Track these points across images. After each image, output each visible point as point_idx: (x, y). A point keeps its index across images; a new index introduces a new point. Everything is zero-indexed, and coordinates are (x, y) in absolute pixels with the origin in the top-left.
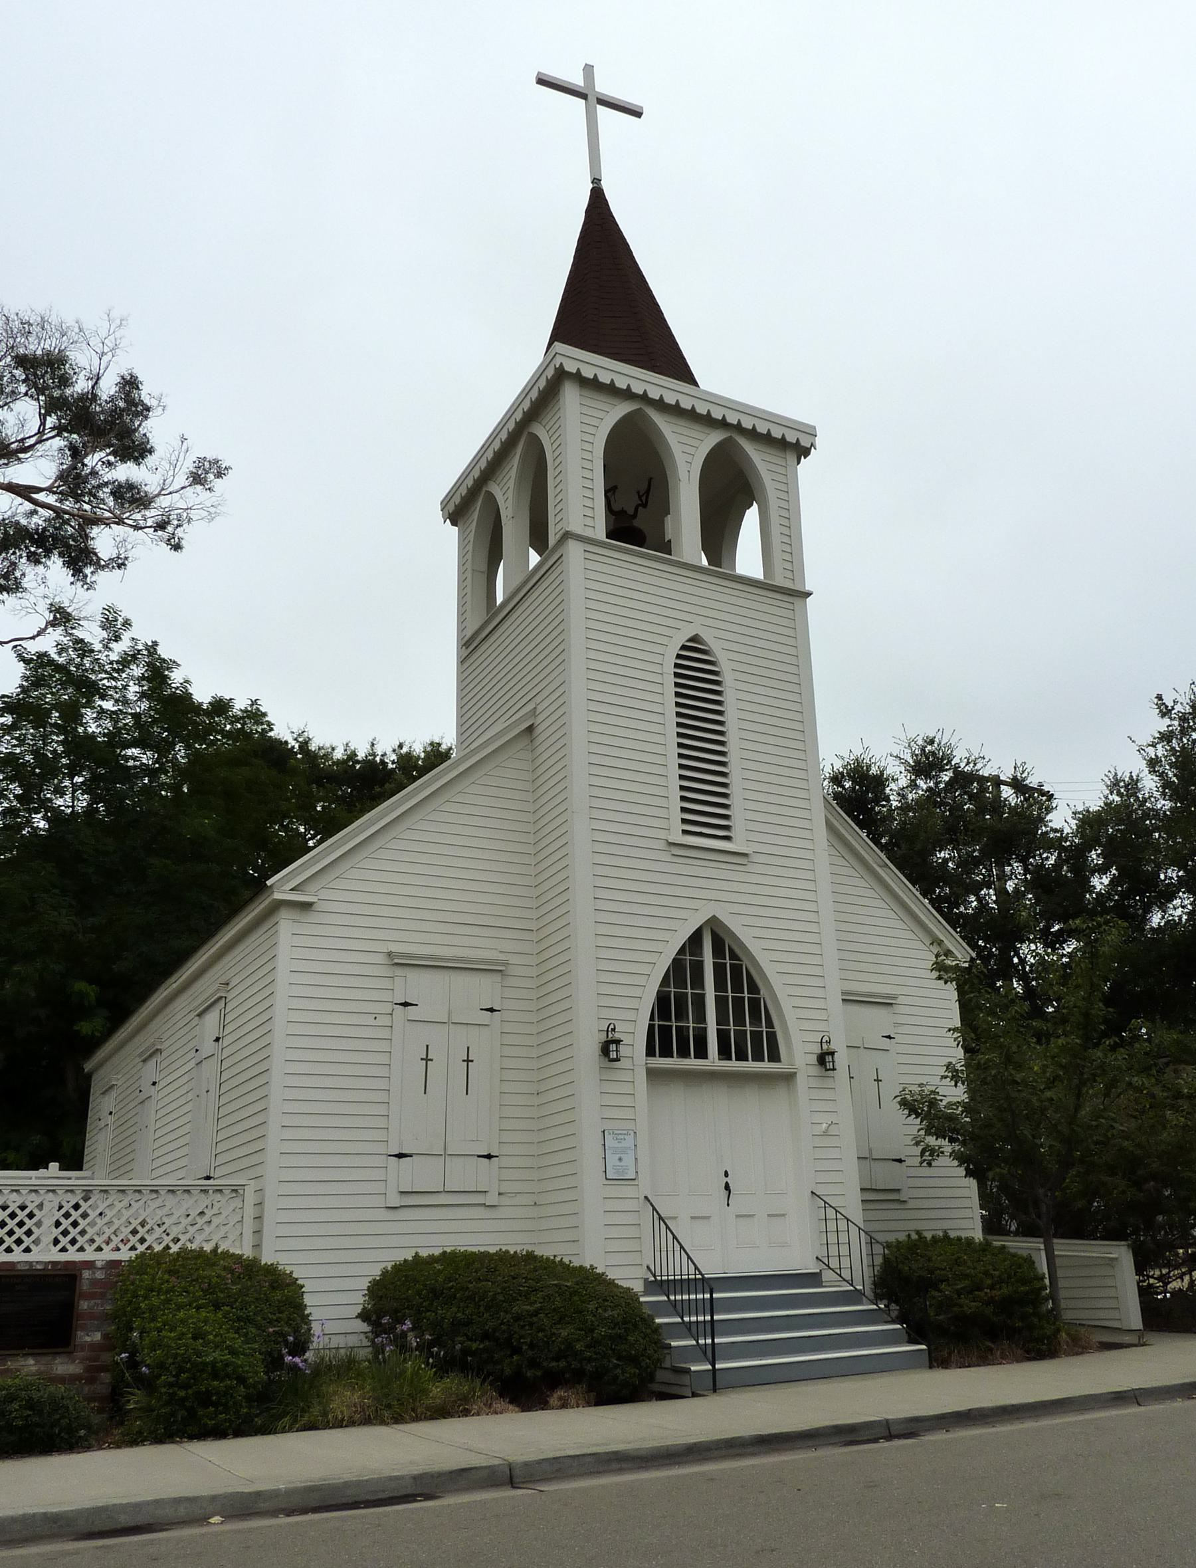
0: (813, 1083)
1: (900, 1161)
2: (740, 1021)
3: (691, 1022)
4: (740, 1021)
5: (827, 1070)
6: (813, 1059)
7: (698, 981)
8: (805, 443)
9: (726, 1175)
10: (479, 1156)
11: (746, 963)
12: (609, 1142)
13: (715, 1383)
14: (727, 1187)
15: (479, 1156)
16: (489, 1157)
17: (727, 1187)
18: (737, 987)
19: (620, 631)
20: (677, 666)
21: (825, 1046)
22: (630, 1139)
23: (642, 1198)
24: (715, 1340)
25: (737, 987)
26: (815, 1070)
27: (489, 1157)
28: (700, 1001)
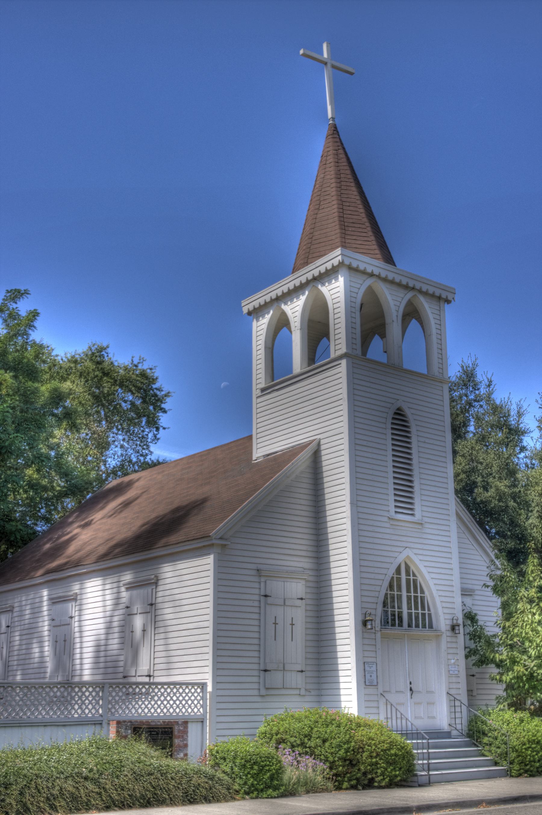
0: (449, 639)
1: (473, 676)
2: (416, 608)
3: (389, 607)
4: (416, 608)
5: (456, 633)
6: (449, 628)
7: (399, 589)
8: (450, 298)
9: (411, 683)
10: (298, 671)
11: (419, 579)
12: (367, 668)
13: (429, 783)
14: (411, 689)
15: (298, 671)
16: (302, 671)
17: (411, 689)
18: (416, 591)
19: (301, 395)
20: (393, 418)
21: (455, 622)
22: (374, 666)
23: (379, 694)
24: (86, 678)
25: (416, 591)
26: (449, 633)
27: (302, 671)
28: (400, 597)
